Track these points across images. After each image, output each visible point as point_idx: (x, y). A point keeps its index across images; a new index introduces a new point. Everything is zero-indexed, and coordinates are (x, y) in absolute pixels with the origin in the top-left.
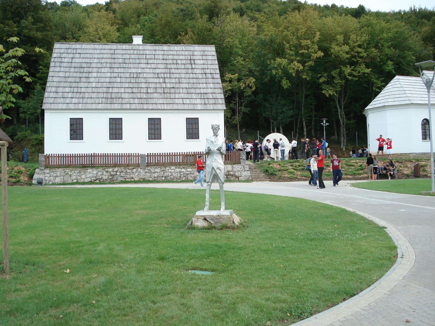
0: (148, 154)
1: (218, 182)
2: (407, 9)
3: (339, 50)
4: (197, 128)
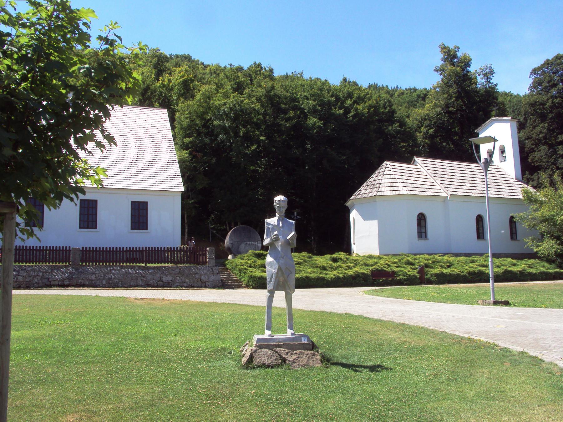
0: (83, 248)
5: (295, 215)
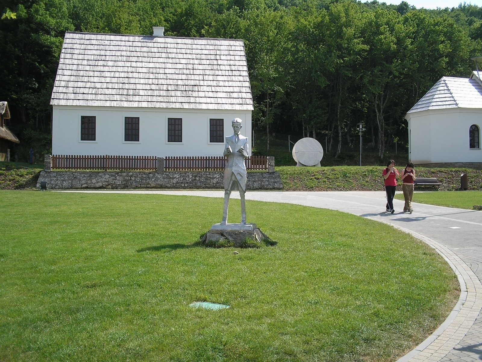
0: (166, 157)
1: (238, 190)
2: (456, 6)
3: (388, 39)
4: (221, 129)
5: (361, 127)
